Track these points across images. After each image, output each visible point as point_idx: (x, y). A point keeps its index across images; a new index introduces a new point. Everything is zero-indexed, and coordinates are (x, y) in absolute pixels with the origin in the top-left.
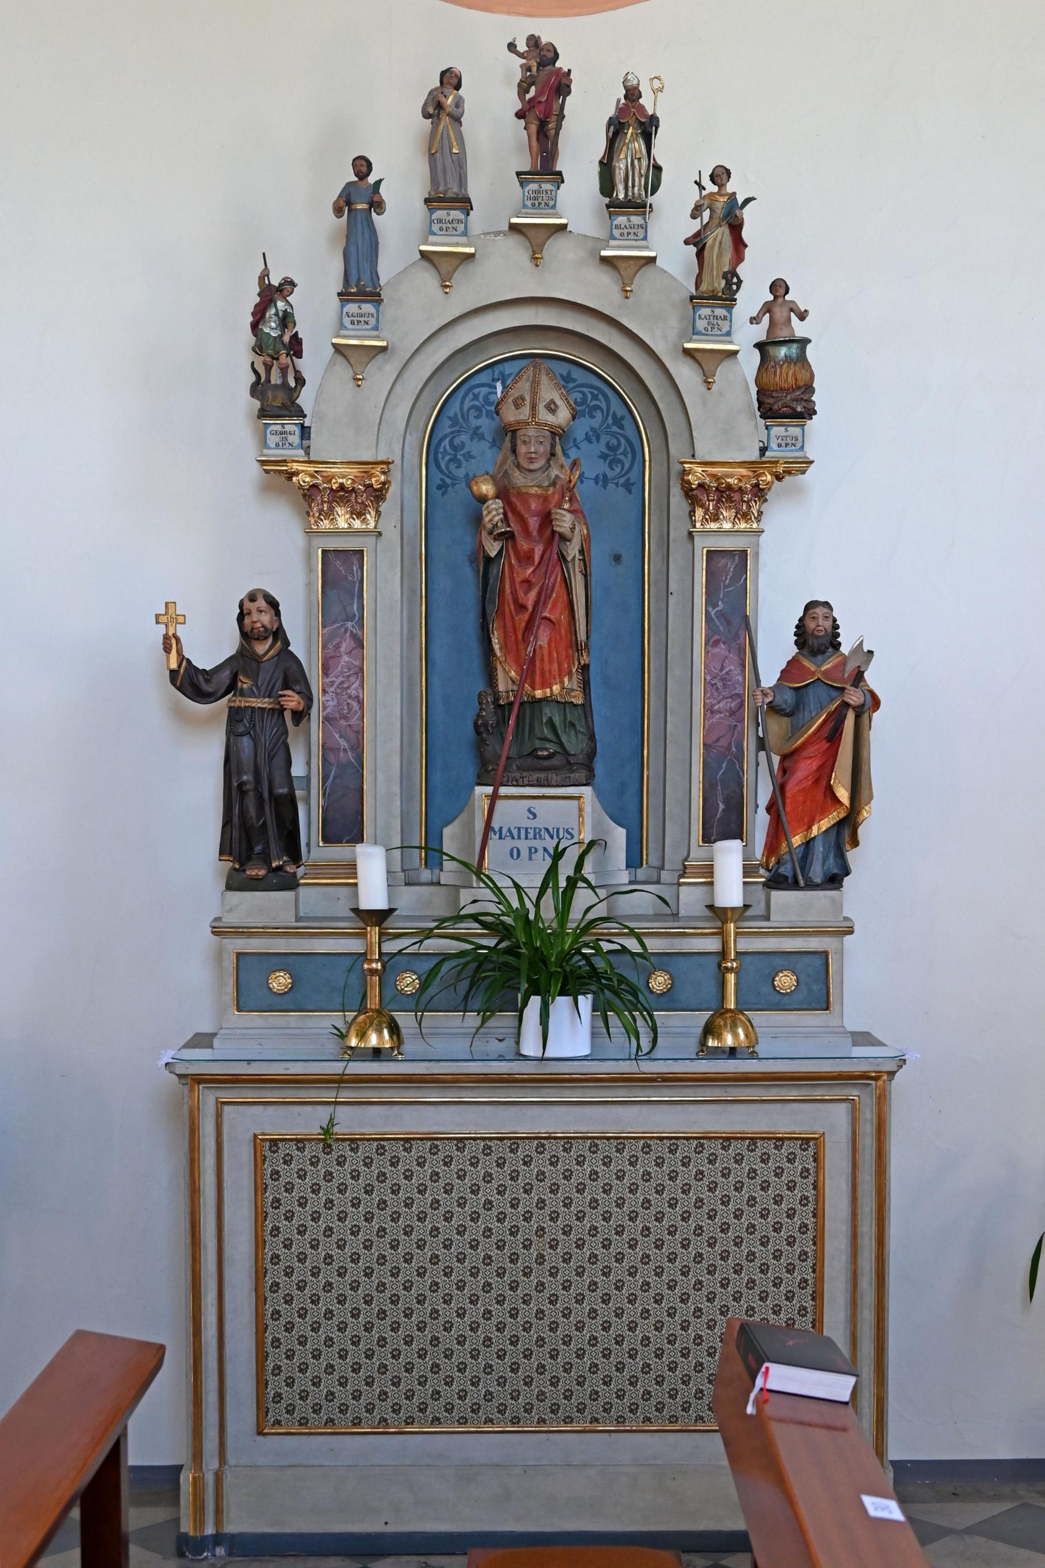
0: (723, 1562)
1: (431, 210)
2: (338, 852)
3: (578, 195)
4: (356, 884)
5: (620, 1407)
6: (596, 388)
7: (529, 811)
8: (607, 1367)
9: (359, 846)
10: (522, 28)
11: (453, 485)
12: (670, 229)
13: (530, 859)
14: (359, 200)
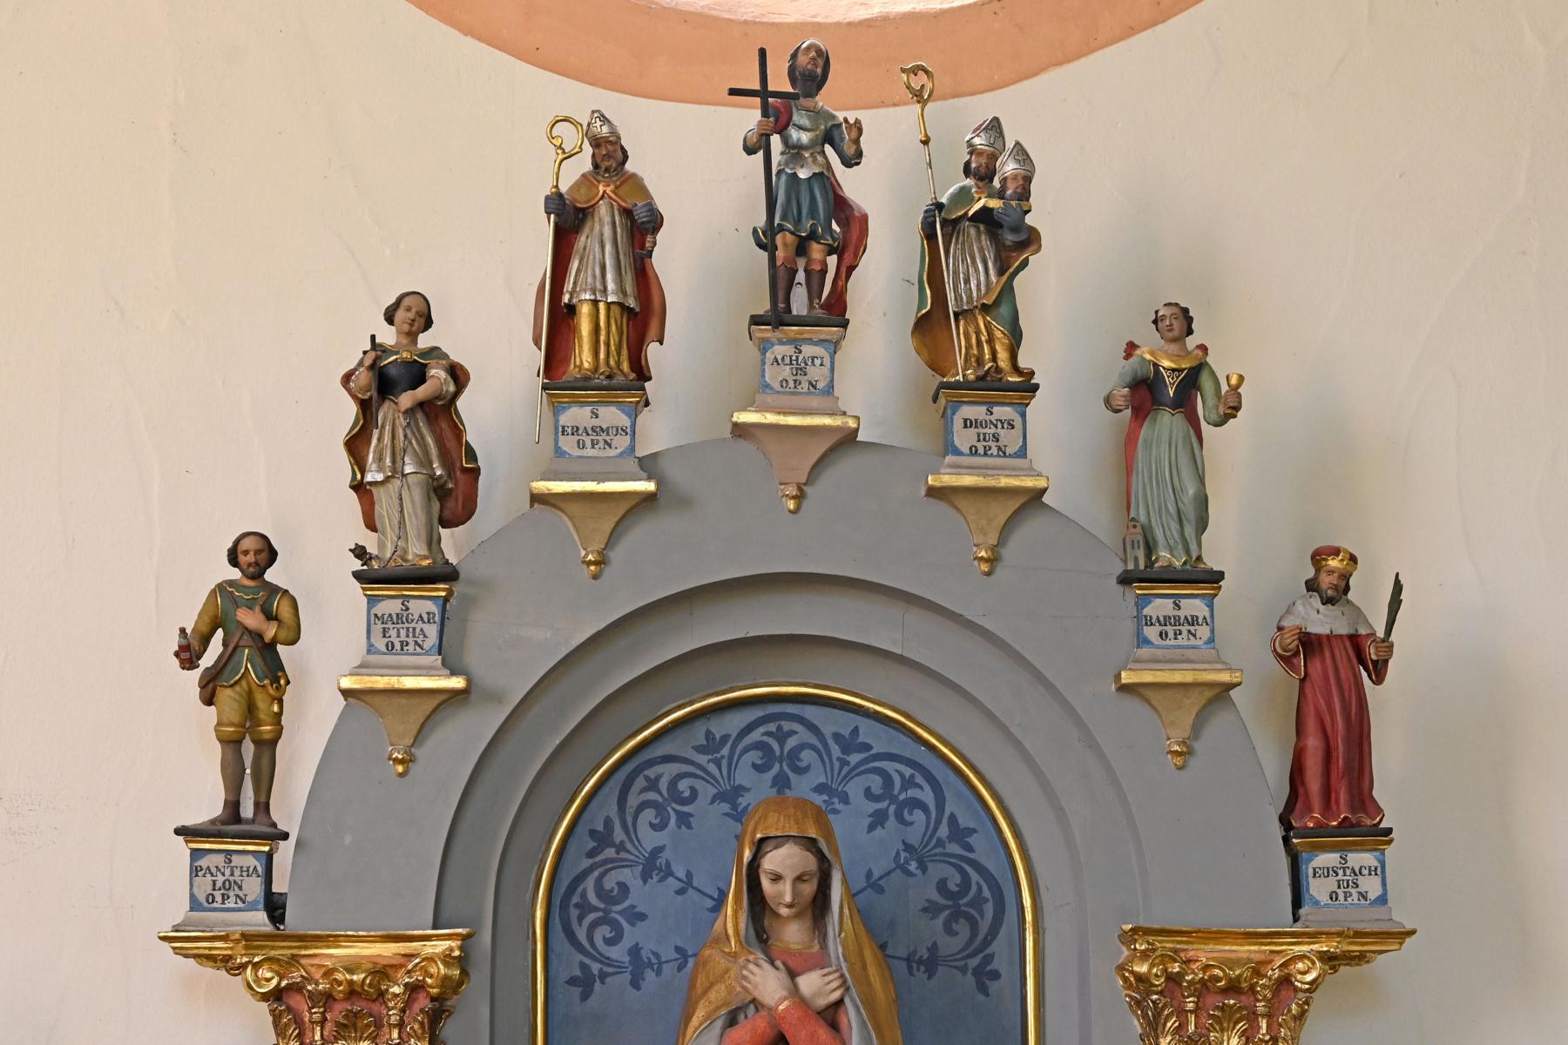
1: (557, 408)
10: (582, 100)
11: (603, 976)
12: (1062, 437)
14: (403, 387)
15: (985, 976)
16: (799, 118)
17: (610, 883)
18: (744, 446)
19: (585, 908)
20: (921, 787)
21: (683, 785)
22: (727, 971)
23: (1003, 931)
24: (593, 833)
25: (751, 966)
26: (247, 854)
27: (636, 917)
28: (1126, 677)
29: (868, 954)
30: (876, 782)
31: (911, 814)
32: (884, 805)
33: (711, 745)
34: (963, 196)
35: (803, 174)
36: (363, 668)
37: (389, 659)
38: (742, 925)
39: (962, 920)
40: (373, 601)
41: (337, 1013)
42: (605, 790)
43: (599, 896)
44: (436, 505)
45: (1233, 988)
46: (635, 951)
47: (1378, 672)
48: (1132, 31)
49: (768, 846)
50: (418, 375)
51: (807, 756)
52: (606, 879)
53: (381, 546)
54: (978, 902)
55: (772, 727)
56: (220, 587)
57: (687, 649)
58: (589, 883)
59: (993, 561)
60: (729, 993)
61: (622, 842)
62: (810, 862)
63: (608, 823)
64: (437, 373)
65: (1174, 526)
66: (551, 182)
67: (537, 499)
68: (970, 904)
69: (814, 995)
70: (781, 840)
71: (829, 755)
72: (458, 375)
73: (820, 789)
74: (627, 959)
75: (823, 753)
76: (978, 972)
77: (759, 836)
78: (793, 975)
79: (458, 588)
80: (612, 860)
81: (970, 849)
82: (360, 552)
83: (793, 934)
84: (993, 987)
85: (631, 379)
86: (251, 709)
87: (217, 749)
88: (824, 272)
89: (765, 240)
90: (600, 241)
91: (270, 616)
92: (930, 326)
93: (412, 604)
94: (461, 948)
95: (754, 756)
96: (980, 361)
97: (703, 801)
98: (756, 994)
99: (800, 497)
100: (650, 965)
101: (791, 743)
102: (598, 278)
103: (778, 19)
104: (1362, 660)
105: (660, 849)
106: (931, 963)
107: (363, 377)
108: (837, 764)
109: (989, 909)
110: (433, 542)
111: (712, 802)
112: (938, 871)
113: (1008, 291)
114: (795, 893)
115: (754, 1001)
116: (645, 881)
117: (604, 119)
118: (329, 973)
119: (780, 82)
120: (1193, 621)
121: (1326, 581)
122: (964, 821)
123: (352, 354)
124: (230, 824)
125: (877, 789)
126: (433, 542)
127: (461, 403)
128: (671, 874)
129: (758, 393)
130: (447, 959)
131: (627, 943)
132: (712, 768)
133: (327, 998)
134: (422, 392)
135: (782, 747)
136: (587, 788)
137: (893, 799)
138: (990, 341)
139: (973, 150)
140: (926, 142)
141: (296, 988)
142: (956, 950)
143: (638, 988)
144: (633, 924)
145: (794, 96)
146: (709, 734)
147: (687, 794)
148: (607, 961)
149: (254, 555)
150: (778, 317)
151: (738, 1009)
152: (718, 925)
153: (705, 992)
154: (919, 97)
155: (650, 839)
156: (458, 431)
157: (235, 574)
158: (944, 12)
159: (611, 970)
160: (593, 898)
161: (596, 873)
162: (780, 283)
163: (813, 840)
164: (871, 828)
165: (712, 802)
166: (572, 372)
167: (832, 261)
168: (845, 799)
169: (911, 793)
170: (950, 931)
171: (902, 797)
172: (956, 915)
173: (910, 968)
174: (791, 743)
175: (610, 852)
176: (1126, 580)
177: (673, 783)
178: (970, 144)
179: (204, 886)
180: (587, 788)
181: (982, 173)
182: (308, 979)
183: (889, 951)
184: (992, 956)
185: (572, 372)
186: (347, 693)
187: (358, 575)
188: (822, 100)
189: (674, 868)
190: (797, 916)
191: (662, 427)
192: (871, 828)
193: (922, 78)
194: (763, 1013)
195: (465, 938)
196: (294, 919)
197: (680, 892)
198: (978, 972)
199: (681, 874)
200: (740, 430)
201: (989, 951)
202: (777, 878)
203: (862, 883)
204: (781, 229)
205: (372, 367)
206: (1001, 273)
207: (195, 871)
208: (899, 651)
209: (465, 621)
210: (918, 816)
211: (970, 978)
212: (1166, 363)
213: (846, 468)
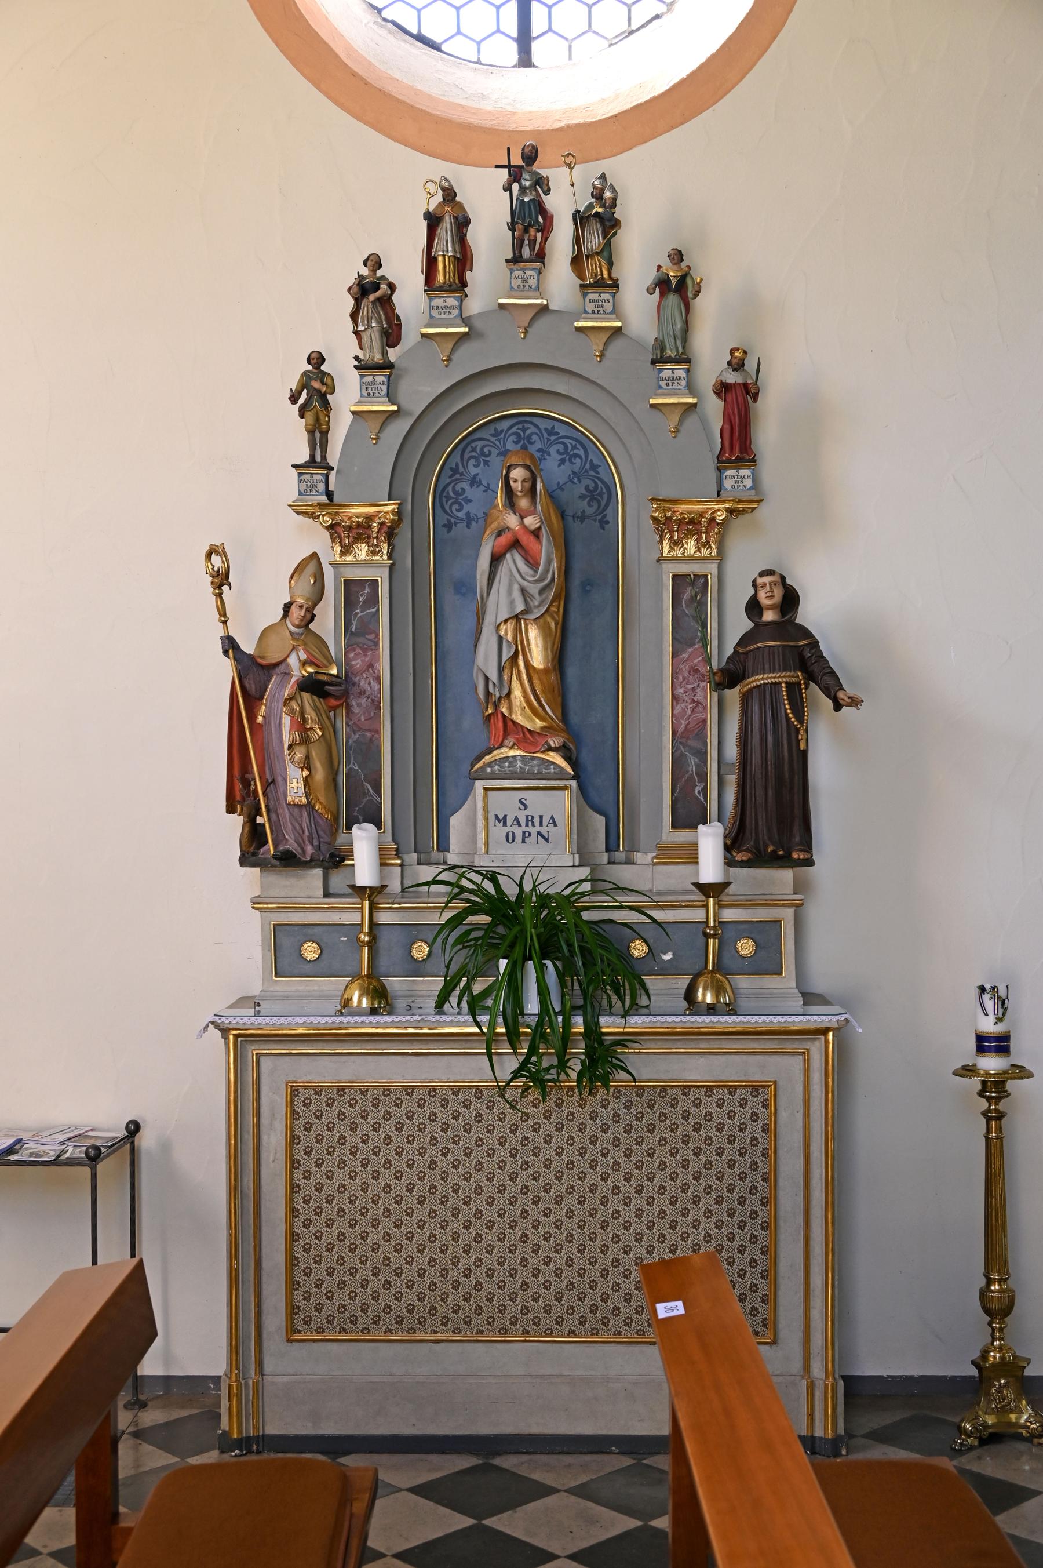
0: (176, 1459)
1: (431, 299)
2: (683, 836)
3: (560, 280)
4: (353, 865)
5: (548, 1321)
6: (575, 440)
7: (520, 801)
8: (582, 1285)
9: (701, 827)
11: (456, 523)
12: (638, 307)
13: (524, 842)
14: (371, 292)
15: (603, 523)
16: (526, 176)
18: (504, 313)
19: (448, 498)
21: (486, 450)
24: (451, 469)
26: (318, 474)
27: (468, 501)
28: (652, 401)
29: (552, 511)
30: (561, 447)
33: (497, 434)
34: (590, 206)
35: (526, 199)
36: (359, 403)
37: (369, 399)
40: (362, 377)
41: (353, 534)
45: (691, 522)
46: (468, 514)
47: (755, 397)
48: (672, 128)
50: (376, 287)
51: (534, 438)
53: (365, 355)
54: (601, 494)
55: (520, 426)
56: (305, 373)
58: (450, 488)
59: (602, 356)
62: (527, 474)
63: (457, 465)
64: (384, 286)
65: (673, 341)
66: (511, 41)
67: (423, 335)
68: (598, 495)
70: (516, 466)
72: (392, 287)
73: (539, 450)
75: (540, 436)
76: (600, 521)
78: (522, 518)
79: (394, 371)
82: (357, 358)
83: (524, 503)
85: (459, 286)
86: (317, 419)
87: (306, 434)
88: (535, 240)
89: (512, 227)
90: (446, 230)
91: (323, 383)
92: (577, 262)
93: (377, 378)
95: (513, 438)
96: (596, 275)
97: (493, 455)
99: (526, 332)
101: (528, 432)
102: (445, 247)
103: (523, 129)
104: (748, 392)
105: (477, 474)
107: (355, 289)
109: (605, 497)
110: (384, 353)
113: (608, 245)
114: (522, 486)
115: (508, 528)
117: (446, 180)
118: (350, 518)
119: (517, 160)
120: (679, 379)
121: (734, 361)
122: (596, 462)
123: (351, 281)
124: (311, 463)
125: (562, 450)
126: (384, 353)
127: (394, 298)
129: (511, 292)
130: (393, 512)
131: (464, 511)
132: (497, 443)
133: (350, 528)
134: (378, 294)
137: (568, 454)
138: (600, 267)
139: (594, 187)
140: (573, 185)
141: (338, 524)
145: (525, 168)
146: (495, 429)
148: (457, 518)
149: (317, 360)
150: (516, 260)
154: (570, 167)
155: (473, 471)
156: (393, 309)
157: (310, 368)
158: (592, 123)
160: (451, 494)
162: (518, 244)
164: (559, 465)
166: (437, 284)
167: (539, 235)
169: (575, 451)
170: (590, 505)
174: (528, 432)
175: (458, 476)
176: (654, 362)
177: (482, 449)
178: (593, 184)
179: (303, 486)
181: (598, 195)
182: (343, 521)
185: (437, 284)
186: (353, 413)
187: (356, 367)
188: (534, 168)
190: (524, 496)
191: (476, 304)
192: (559, 465)
193: (571, 158)
195: (399, 504)
196: (337, 499)
198: (600, 521)
200: (502, 306)
202: (515, 481)
203: (555, 487)
204: (517, 223)
205: (358, 285)
206: (604, 238)
207: (300, 481)
210: (578, 460)
211: (597, 524)
212: (672, 274)
213: (543, 322)
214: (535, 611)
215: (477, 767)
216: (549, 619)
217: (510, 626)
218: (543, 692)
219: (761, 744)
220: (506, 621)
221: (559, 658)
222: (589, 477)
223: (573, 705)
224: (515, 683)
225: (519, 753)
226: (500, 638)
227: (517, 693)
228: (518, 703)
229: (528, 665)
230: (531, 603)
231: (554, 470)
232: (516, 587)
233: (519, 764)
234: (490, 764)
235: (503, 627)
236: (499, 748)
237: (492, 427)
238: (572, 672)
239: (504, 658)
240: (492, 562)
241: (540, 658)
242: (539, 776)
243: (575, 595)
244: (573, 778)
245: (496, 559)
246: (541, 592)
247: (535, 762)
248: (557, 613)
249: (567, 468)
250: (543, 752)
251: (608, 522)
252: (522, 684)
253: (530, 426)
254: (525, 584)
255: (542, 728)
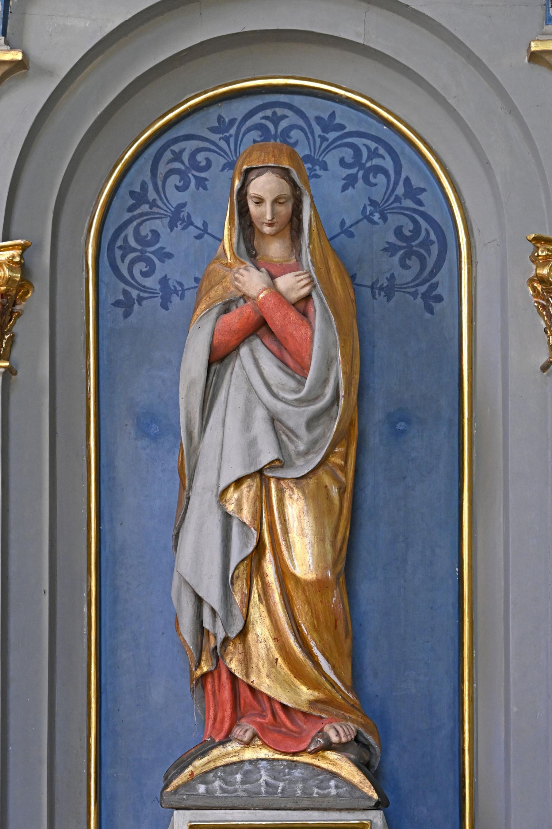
11: (140, 300)
15: (431, 299)
17: (145, 231)
19: (126, 249)
20: (383, 158)
21: (201, 158)
22: (224, 277)
23: (446, 264)
24: (132, 194)
25: (241, 271)
28: (534, 47)
30: (348, 154)
31: (375, 177)
32: (353, 171)
38: (235, 240)
39: (414, 257)
42: (141, 161)
43: (137, 240)
44: (269, 517)
46: (164, 281)
49: (252, 176)
52: (142, 228)
54: (426, 244)
55: (269, 113)
57: (198, 41)
58: (130, 230)
60: (225, 292)
61: (154, 200)
63: (144, 185)
68: (421, 245)
69: (288, 289)
70: (262, 170)
71: (312, 133)
74: (158, 287)
75: (308, 132)
76: (425, 296)
77: (245, 167)
78: (273, 277)
80: (147, 214)
81: (420, 203)
83: (276, 250)
84: (437, 307)
94: (21, 256)
97: (215, 168)
98: (244, 289)
100: (176, 291)
101: (283, 124)
105: (183, 205)
106: (389, 292)
108: (318, 141)
109: (435, 249)
111: (223, 170)
112: (394, 220)
114: (274, 214)
115: (245, 297)
116: (172, 230)
122: (416, 182)
125: (349, 159)
128: (192, 224)
132: (223, 144)
135: (276, 128)
136: (127, 157)
137: (362, 166)
142: (410, 279)
143: (167, 309)
144: (162, 261)
147: (203, 163)
148: (144, 289)
151: (230, 302)
152: (220, 249)
153: (207, 292)
155: (176, 198)
159: (146, 295)
160: (133, 243)
161: (135, 223)
163: (287, 171)
164: (344, 188)
165: (223, 170)
168: (325, 167)
169: (376, 161)
170: (404, 265)
171: (368, 165)
172: (409, 254)
173: (373, 294)
174: (283, 124)
175: (145, 208)
177: (193, 155)
180: (127, 157)
183: (357, 281)
184: (437, 284)
189: (193, 219)
192: (344, 188)
194: (249, 303)
195: (24, 248)
197: (198, 237)
198: (425, 296)
199: (199, 224)
201: (434, 280)
202: (260, 201)
203: (337, 230)
208: (361, 41)
209: (24, 14)
210: (381, 178)
211: (419, 301)
214: (300, 462)
215: (176, 782)
216: (327, 480)
217: (248, 492)
218: (316, 629)
219: (459, 716)
220: (238, 482)
221: (346, 559)
222: (401, 211)
223: (371, 657)
224: (258, 611)
225: (264, 753)
226: (227, 517)
227: (261, 630)
228: (263, 652)
229: (283, 573)
230: (291, 447)
231: (332, 197)
232: (260, 414)
233: (264, 777)
234: (203, 777)
235: (233, 495)
236: (223, 743)
237: (214, 112)
238: (368, 590)
239: (235, 559)
240: (210, 364)
241: (309, 559)
242: (306, 803)
243: (374, 440)
244: (377, 806)
245: (219, 358)
246: (312, 423)
247: (297, 773)
248: (343, 468)
249: (359, 193)
250: (315, 753)
251: (439, 299)
252: (270, 612)
253: (287, 112)
254: (280, 406)
255: (313, 703)
